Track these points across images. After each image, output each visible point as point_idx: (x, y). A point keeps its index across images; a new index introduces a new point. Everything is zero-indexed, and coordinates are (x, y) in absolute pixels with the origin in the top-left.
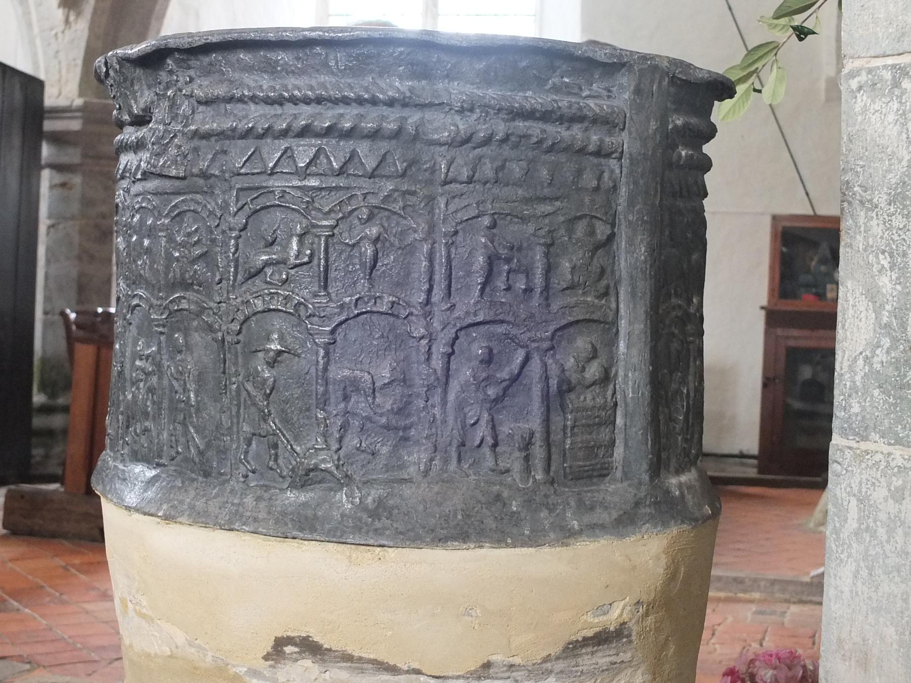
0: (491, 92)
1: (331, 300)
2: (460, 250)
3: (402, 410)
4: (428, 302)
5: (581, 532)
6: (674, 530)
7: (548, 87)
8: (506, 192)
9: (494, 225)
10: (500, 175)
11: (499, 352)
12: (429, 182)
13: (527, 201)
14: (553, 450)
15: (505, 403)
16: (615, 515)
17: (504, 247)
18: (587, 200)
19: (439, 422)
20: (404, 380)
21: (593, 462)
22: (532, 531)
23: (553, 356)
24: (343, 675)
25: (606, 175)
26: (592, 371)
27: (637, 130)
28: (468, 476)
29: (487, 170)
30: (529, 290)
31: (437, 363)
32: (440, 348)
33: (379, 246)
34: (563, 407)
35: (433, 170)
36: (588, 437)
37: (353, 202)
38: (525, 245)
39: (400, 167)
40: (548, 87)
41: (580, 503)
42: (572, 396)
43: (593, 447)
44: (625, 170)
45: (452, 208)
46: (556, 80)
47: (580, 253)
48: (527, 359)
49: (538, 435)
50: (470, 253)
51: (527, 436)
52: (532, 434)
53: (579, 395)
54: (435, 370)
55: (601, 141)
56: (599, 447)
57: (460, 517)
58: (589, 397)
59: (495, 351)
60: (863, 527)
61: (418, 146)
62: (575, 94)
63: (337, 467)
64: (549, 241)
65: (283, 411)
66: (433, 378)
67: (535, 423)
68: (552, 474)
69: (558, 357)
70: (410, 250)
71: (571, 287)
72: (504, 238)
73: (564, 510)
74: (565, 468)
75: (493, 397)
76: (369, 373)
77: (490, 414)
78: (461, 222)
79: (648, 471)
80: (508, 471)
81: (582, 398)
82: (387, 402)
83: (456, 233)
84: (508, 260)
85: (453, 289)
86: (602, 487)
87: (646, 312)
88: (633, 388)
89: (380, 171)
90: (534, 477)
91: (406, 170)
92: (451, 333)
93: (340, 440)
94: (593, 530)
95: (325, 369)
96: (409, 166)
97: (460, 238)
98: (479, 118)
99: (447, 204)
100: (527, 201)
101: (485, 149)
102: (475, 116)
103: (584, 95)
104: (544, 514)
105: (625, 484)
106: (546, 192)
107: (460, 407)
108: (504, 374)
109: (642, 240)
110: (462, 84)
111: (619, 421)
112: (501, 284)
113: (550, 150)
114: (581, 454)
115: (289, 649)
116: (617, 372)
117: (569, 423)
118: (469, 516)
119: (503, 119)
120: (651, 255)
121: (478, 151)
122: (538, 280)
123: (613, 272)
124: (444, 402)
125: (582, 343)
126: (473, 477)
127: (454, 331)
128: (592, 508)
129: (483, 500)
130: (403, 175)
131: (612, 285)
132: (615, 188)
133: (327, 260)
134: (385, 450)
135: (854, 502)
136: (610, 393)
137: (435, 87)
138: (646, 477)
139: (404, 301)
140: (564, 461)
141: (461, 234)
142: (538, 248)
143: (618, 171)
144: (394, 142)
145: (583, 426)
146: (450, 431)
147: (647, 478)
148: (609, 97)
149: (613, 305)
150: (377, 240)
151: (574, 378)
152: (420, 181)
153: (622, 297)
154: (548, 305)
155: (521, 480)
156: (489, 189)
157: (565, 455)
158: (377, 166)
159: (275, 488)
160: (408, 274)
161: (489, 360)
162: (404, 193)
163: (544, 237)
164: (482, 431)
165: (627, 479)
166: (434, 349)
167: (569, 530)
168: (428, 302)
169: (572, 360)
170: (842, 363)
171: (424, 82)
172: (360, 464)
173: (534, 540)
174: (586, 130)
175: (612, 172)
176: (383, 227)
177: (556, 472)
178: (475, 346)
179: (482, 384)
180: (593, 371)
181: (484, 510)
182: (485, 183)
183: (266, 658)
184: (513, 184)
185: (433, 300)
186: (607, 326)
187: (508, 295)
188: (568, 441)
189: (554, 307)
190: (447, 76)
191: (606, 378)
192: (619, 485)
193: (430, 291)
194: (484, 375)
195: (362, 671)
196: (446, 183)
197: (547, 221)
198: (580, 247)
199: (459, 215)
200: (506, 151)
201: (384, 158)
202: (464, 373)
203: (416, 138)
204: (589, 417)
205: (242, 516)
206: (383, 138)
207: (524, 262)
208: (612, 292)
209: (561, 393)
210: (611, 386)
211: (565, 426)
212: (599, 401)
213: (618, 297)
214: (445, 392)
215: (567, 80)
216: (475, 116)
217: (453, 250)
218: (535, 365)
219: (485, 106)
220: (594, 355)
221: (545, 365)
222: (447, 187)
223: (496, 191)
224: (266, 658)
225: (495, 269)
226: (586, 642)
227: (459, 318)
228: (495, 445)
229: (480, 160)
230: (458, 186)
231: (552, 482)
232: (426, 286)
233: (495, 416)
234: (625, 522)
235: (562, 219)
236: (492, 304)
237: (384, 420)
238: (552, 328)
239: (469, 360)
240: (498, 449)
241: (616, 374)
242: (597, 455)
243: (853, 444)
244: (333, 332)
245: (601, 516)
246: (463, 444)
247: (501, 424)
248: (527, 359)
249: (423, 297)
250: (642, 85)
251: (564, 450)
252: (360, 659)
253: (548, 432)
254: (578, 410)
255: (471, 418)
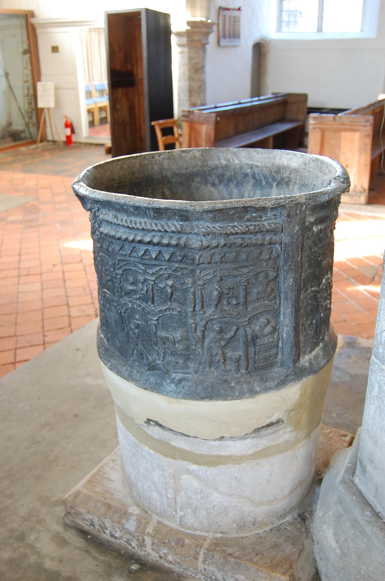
0: (217, 225)
1: (156, 308)
2: (206, 291)
3: (187, 348)
4: (194, 310)
5: (260, 392)
6: (304, 380)
7: (245, 220)
8: (228, 266)
9: (221, 280)
10: (223, 259)
11: (226, 328)
12: (193, 264)
13: (235, 269)
14: (250, 360)
15: (229, 346)
16: (276, 382)
17: (226, 289)
18: (264, 264)
19: (201, 355)
20: (186, 339)
21: (268, 362)
22: (239, 394)
23: (250, 327)
24: (171, 434)
25: (274, 251)
26: (267, 329)
27: (288, 232)
28: (213, 373)
29: (217, 258)
30: (238, 304)
31: (199, 333)
32: (200, 328)
33: (173, 288)
34: (254, 345)
35: (193, 259)
36: (266, 354)
37: (161, 271)
38: (236, 286)
39: (180, 258)
40: (245, 220)
41: (262, 379)
42: (258, 340)
43: (268, 357)
44: (283, 249)
45: (202, 275)
46: (248, 216)
47: (261, 286)
48: (238, 329)
49: (243, 357)
50: (211, 292)
51: (238, 358)
52: (240, 357)
53: (262, 339)
54: (198, 336)
55: (271, 239)
56: (270, 356)
57: (210, 389)
58: (266, 339)
59: (224, 328)
60: (379, 396)
61: (186, 250)
62: (258, 221)
63: (164, 367)
64: (246, 284)
65: (143, 344)
66: (197, 339)
67: (241, 353)
68: (249, 369)
69: (252, 326)
70: (186, 290)
71: (258, 299)
72: (226, 285)
73: (254, 383)
74: (255, 367)
75: (223, 345)
76: (172, 336)
77: (222, 351)
78: (207, 280)
79: (292, 363)
80: (230, 370)
81: (263, 340)
82: (180, 347)
83: (204, 284)
84: (227, 294)
85: (205, 305)
86: (272, 370)
87: (292, 304)
88: (286, 333)
89: (170, 260)
90: (241, 372)
91: (182, 260)
92: (203, 323)
93: (164, 358)
94: (266, 390)
95: (156, 333)
96: (183, 258)
97: (206, 286)
98: (212, 238)
99: (200, 273)
100: (235, 269)
101: (216, 249)
102: (210, 237)
103: (262, 220)
104: (245, 386)
105: (282, 368)
106: (245, 263)
107: (210, 348)
108: (228, 336)
109: (291, 277)
110: (204, 222)
111: (280, 345)
112: (225, 302)
113: (245, 247)
114: (262, 361)
115: (151, 423)
116: (279, 327)
117: (257, 350)
118: (213, 389)
119: (223, 237)
120: (295, 282)
121: (213, 250)
122: (242, 300)
123: (278, 289)
124: (202, 347)
125: (263, 320)
126: (216, 373)
127: (205, 321)
128: (266, 381)
129: (219, 382)
130: (181, 261)
131: (277, 294)
132: (278, 256)
133: (153, 294)
134: (181, 362)
135: (377, 386)
136: (276, 335)
137: (192, 224)
138: (291, 365)
139: (184, 310)
140: (255, 364)
141: (206, 284)
142: (241, 287)
143: (280, 249)
144: (176, 248)
145: (263, 350)
146: (206, 357)
147: (292, 366)
148: (275, 219)
149: (278, 302)
150: (172, 287)
151: (259, 334)
152: (188, 264)
153: (282, 298)
154: (247, 308)
155: (236, 373)
156: (218, 265)
157: (255, 361)
158: (170, 258)
159: (144, 368)
160: (186, 300)
161: (221, 331)
162: (182, 269)
163: (244, 283)
164: (219, 357)
165: (283, 366)
166: (198, 328)
167: (255, 392)
168: (194, 310)
169: (258, 327)
170: (377, 330)
171: (187, 222)
172: (172, 366)
173: (240, 396)
174: (264, 235)
175: (277, 250)
176: (174, 281)
177: (251, 369)
178: (215, 327)
179: (217, 341)
180: (268, 329)
181: (220, 386)
182: (217, 263)
183: (145, 422)
184: (229, 262)
185: (197, 309)
186: (276, 313)
187: (229, 306)
188: (257, 357)
189: (250, 309)
190: (197, 220)
191: (275, 329)
192: (279, 369)
193: (195, 307)
194: (219, 337)
195: (177, 435)
196: (198, 265)
197: (245, 275)
198: (261, 284)
199: (206, 277)
200: (226, 249)
201: (172, 254)
202: (210, 336)
203: (185, 246)
204: (265, 347)
205: (132, 377)
206: (171, 246)
207: (236, 293)
208: (278, 297)
209: (253, 340)
210: (277, 333)
211: (255, 351)
212: (271, 340)
213: (280, 299)
214: (203, 343)
215: (254, 215)
216: (210, 237)
217: (203, 291)
218: (241, 332)
219: (214, 233)
220: (269, 322)
221: (246, 331)
222: (200, 266)
223: (222, 266)
224: (145, 422)
225: (222, 297)
226: (263, 427)
227: (207, 317)
228: (225, 361)
229: (213, 254)
230: (204, 265)
231: (249, 373)
232: (193, 305)
233: (225, 351)
234: (282, 383)
235: (252, 274)
236: (221, 311)
237: (179, 352)
238: (248, 317)
239: (213, 331)
240: (226, 362)
241: (279, 328)
242: (270, 360)
243: (379, 363)
244: (157, 320)
245: (270, 384)
246: (211, 362)
247: (227, 353)
248: (238, 329)
249: (191, 310)
250: (291, 213)
251: (255, 360)
252: (176, 431)
253: (247, 355)
254: (261, 345)
255: (214, 352)
